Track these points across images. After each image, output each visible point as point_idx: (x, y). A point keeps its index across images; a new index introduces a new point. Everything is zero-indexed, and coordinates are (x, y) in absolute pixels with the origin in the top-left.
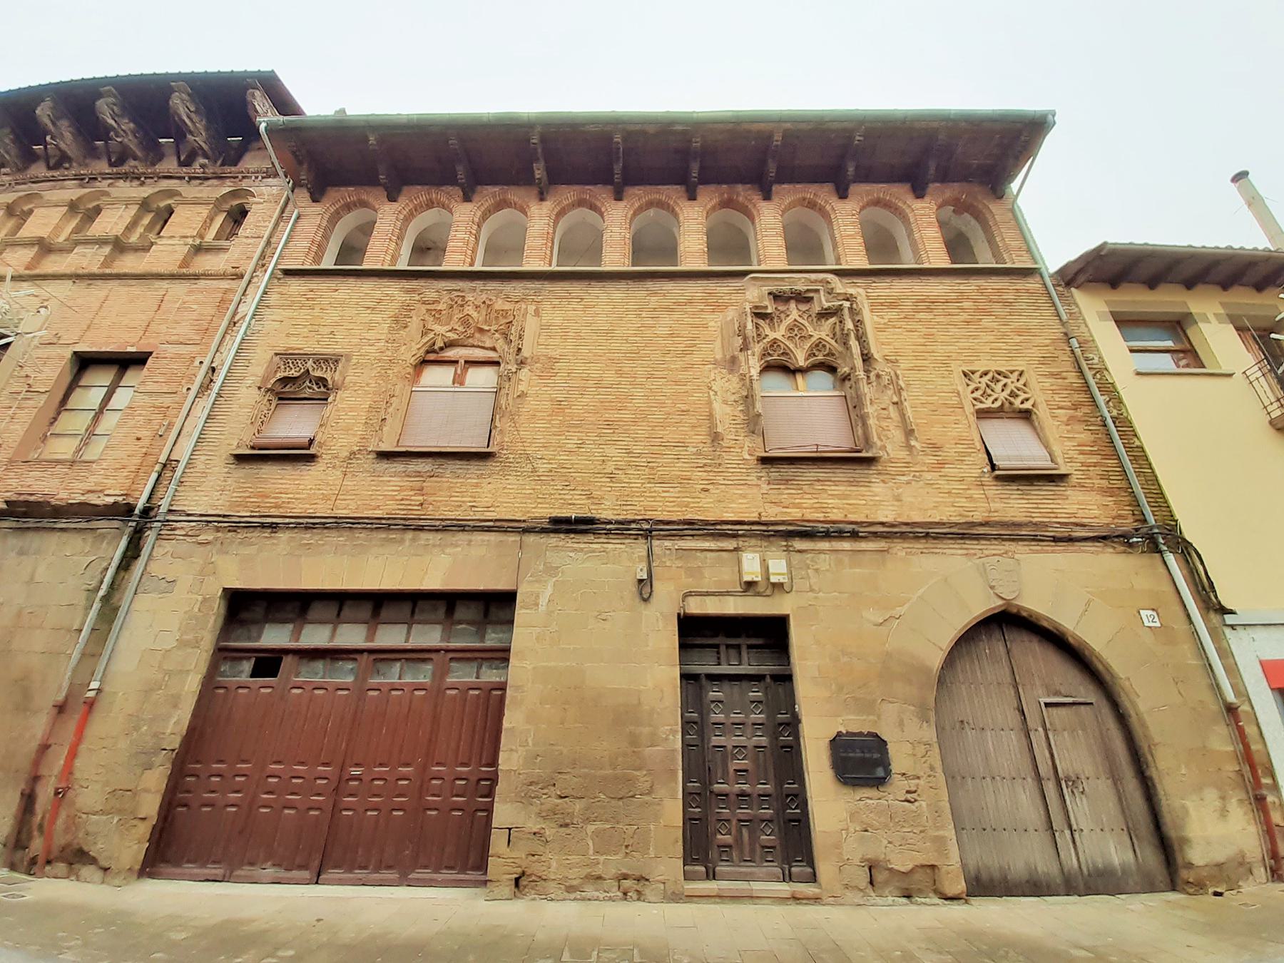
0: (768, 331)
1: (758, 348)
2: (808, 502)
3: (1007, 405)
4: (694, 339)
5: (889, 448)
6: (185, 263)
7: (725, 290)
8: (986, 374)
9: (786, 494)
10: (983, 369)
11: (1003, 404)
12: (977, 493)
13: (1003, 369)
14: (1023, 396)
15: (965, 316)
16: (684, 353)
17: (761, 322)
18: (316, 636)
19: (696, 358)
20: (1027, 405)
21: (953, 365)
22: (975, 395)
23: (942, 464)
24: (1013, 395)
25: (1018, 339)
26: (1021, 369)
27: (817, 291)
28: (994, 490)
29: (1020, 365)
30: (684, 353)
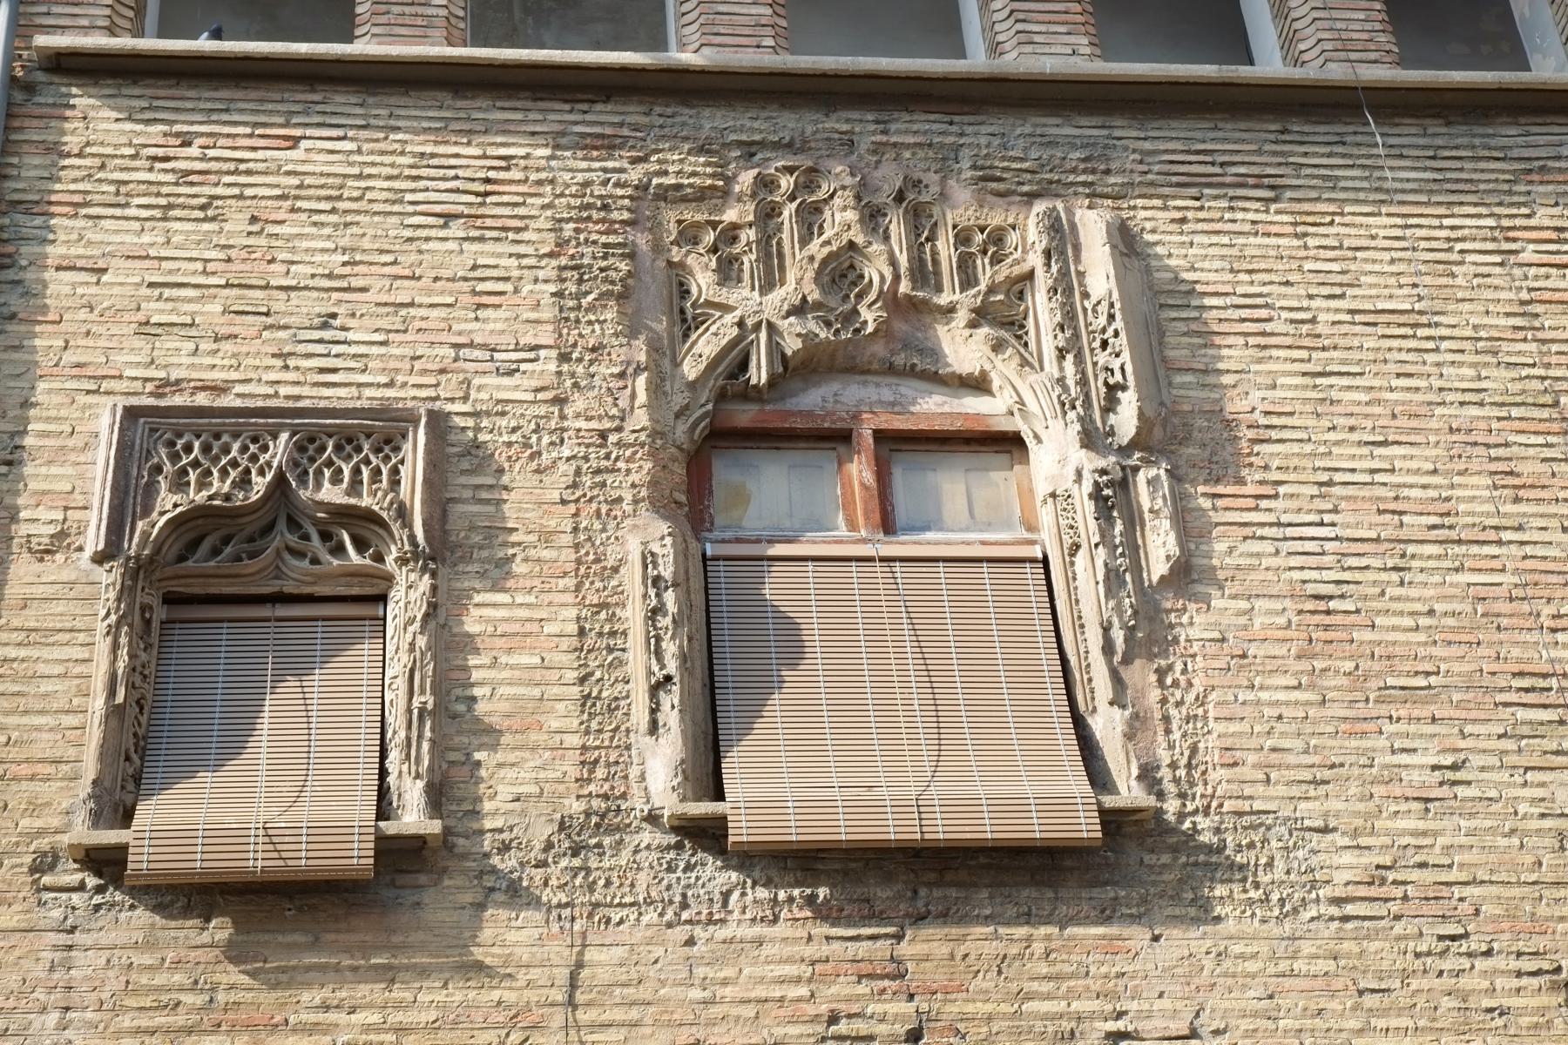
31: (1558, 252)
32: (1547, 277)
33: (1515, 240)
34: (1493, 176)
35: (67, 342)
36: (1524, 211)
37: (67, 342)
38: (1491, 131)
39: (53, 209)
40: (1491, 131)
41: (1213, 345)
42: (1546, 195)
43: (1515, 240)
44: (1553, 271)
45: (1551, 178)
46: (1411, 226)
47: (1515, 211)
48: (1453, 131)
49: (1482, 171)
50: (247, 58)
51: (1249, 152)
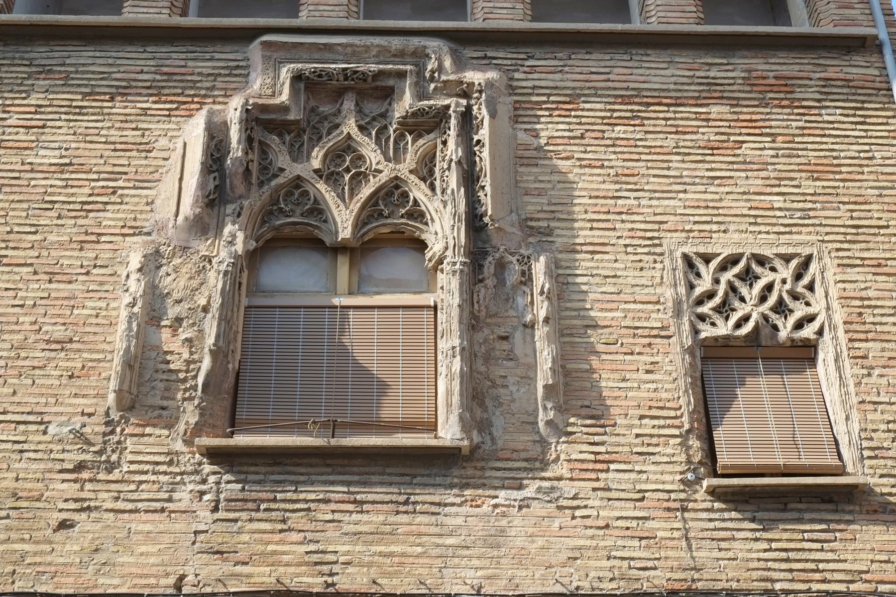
0: (282, 159)
1: (255, 200)
2: (294, 549)
4: (115, 175)
5: (498, 422)
6: (47, 427)
7: (205, 67)
8: (733, 260)
9: (251, 533)
10: (726, 252)
11: (756, 328)
12: (660, 527)
13: (768, 252)
14: (800, 311)
15: (709, 135)
16: (86, 209)
17: (274, 140)
18: (523, 106)
19: (111, 218)
21: (670, 241)
22: (701, 310)
23: (603, 463)
24: (781, 308)
25: (809, 186)
26: (806, 251)
27: (402, 75)
28: (706, 517)
29: (803, 242)
30: (86, 209)
31: (31, 119)
32: (17, 133)
33: (9, 112)
34: (14, 75)
35: (34, 382)
36: (24, 95)
37: (34, 382)
38: (29, 49)
39: (578, 248)
40: (29, 49)
41: (572, 229)
42: (43, 86)
43: (9, 112)
44: (22, 130)
45: (52, 76)
46: (113, 114)
47: (17, 95)
48: (7, 49)
49: (11, 72)
50: (578, 32)
51: (876, 109)
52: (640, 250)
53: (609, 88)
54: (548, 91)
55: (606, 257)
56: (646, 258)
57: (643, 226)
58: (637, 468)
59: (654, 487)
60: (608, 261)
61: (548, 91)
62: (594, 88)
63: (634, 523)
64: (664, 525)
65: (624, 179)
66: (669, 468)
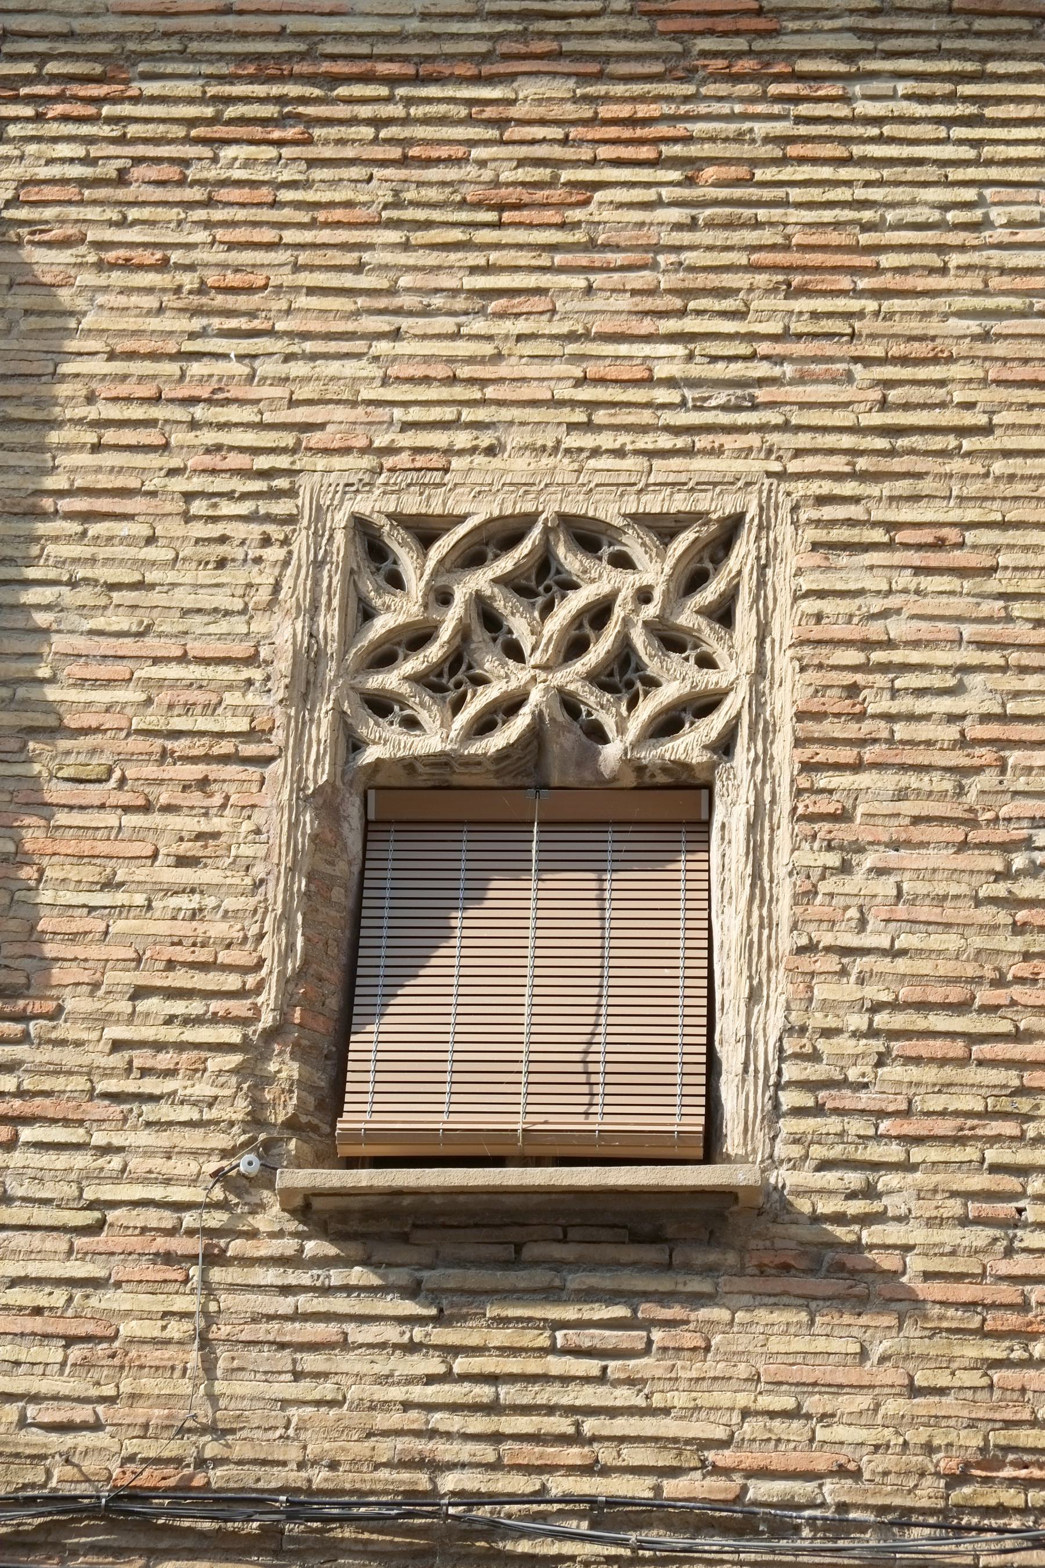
3: (565, 741)
10: (482, 511)
11: (536, 733)
13: (608, 510)
14: (675, 680)
20: (689, 746)
25: (769, 314)
26: (726, 505)
29: (721, 478)
52: (227, 508)
53: (226, 35)
54: (41, 46)
55: (124, 529)
56: (238, 530)
57: (249, 438)
58: (99, 1139)
59: (137, 1192)
60: (128, 541)
61: (41, 46)
62: (184, 35)
63: (59, 1297)
64: (145, 1302)
65: (220, 300)
66: (194, 1139)
